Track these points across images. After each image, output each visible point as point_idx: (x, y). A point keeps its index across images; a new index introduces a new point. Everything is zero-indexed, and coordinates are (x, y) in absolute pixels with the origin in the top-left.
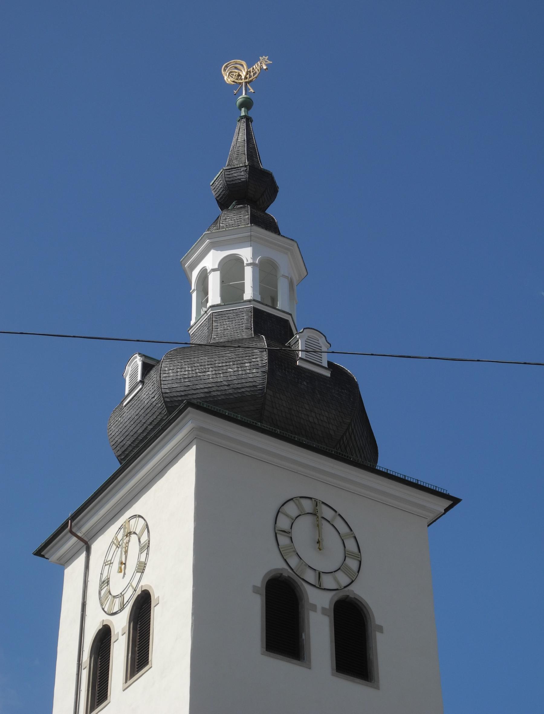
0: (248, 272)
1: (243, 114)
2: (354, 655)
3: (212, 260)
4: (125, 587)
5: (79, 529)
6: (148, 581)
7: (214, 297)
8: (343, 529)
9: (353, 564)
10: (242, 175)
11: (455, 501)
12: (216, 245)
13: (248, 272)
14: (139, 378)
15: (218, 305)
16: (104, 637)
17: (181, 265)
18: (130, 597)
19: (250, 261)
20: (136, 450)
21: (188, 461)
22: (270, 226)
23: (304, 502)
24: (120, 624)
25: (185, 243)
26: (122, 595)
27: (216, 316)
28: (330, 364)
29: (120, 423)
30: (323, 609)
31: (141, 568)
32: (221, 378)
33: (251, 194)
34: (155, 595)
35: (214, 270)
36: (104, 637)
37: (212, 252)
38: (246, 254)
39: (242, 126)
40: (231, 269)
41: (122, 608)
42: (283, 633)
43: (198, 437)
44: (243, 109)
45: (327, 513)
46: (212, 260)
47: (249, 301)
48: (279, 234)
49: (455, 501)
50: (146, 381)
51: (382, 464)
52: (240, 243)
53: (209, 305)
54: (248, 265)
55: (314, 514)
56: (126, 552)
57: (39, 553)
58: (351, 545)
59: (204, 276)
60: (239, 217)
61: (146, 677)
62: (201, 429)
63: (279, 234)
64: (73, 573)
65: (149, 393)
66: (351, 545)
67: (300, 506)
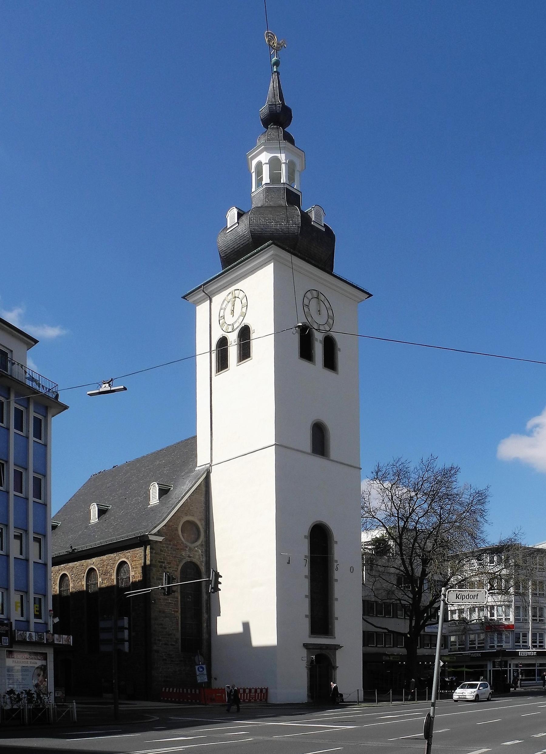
0: (283, 166)
1: (275, 70)
2: (330, 362)
3: (264, 157)
4: (235, 322)
5: (206, 290)
6: (246, 322)
7: (266, 179)
8: (328, 305)
9: (331, 321)
10: (279, 109)
11: (370, 295)
12: (267, 150)
13: (283, 166)
14: (236, 221)
15: (268, 184)
16: (223, 342)
17: (246, 157)
18: (238, 326)
19: (284, 161)
20: (236, 257)
21: (269, 269)
22: (288, 138)
23: (314, 292)
24: (233, 338)
25: (251, 145)
26: (233, 325)
27: (268, 190)
28: (325, 226)
29: (224, 240)
30: (317, 341)
31: (244, 315)
32: (278, 227)
33: (279, 118)
34: (252, 328)
35: (266, 163)
36: (223, 342)
37: (265, 153)
38: (282, 157)
39: (275, 76)
40: (274, 163)
41: (233, 330)
42: (306, 352)
43: (274, 259)
44: (275, 67)
45: (322, 298)
46: (264, 157)
47: (284, 183)
48: (294, 145)
49: (370, 295)
50: (240, 223)
51: (335, 271)
52: (280, 151)
53: (263, 183)
54: (284, 163)
55: (317, 298)
56: (234, 305)
57: (184, 298)
58: (330, 312)
59: (259, 165)
60: (274, 132)
61: (247, 364)
62: (276, 255)
63: (294, 145)
64: (202, 310)
65: (243, 228)
66: (330, 312)
67: (312, 294)
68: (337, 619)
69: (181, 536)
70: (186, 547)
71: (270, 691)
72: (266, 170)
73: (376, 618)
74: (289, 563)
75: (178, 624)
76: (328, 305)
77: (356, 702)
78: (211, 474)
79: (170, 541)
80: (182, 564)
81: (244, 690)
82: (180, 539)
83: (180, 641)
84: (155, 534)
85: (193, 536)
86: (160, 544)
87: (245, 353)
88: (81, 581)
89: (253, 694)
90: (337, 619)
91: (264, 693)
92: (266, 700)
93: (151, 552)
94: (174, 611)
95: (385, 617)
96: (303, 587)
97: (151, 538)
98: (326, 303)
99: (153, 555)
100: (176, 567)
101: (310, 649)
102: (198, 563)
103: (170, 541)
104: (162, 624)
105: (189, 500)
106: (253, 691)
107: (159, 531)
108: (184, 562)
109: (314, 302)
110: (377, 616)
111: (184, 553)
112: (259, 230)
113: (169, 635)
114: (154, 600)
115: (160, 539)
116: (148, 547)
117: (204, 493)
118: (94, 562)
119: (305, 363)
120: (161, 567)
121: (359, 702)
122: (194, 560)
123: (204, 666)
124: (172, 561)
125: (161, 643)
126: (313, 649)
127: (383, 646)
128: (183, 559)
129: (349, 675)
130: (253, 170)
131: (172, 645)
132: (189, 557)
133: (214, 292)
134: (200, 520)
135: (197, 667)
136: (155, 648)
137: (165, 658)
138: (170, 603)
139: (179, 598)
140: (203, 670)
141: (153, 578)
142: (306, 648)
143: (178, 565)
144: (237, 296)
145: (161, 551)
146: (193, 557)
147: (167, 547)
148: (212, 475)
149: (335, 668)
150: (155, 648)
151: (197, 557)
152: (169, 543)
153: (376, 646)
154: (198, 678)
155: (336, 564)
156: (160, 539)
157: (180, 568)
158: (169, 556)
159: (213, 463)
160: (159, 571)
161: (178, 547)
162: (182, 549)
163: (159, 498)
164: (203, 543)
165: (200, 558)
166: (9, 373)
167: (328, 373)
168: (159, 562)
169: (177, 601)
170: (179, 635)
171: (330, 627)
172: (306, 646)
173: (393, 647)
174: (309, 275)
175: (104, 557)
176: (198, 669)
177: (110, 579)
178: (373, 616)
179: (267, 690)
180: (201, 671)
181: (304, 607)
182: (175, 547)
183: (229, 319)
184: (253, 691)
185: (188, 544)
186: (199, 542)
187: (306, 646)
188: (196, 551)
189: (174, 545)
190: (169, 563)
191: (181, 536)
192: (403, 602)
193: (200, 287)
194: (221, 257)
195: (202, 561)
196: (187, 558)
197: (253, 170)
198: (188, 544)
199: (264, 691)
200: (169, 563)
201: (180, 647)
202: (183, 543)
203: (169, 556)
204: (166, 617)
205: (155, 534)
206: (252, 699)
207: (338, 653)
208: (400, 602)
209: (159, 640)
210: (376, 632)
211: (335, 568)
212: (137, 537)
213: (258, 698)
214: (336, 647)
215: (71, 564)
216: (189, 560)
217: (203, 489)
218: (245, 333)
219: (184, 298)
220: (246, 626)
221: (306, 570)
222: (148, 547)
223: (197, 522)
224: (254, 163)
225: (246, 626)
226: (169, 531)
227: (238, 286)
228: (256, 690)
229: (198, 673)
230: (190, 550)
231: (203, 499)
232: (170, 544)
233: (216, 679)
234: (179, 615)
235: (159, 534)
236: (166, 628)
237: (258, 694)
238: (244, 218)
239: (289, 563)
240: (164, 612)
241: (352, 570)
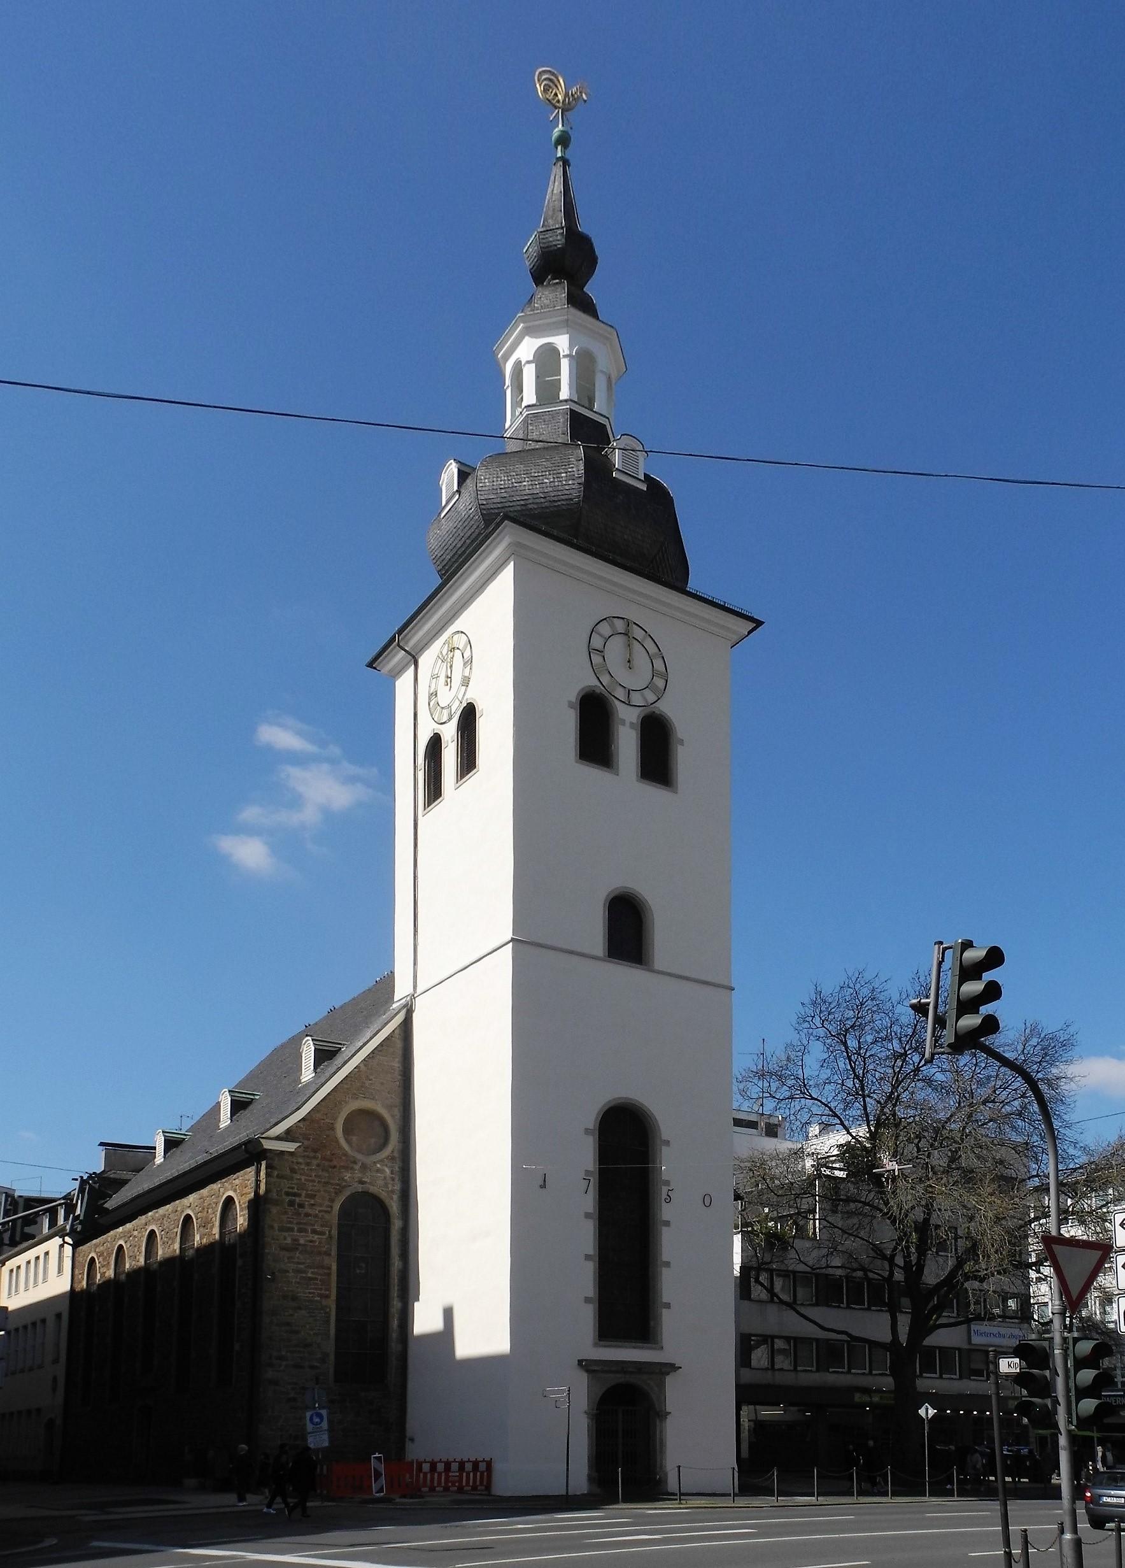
2: (657, 763)
5: (407, 643)
7: (530, 396)
8: (652, 649)
9: (660, 683)
16: (435, 743)
20: (455, 564)
26: (449, 707)
29: (439, 535)
30: (632, 723)
31: (466, 682)
35: (528, 362)
36: (435, 743)
42: (595, 745)
43: (516, 552)
45: (638, 633)
46: (527, 349)
50: (463, 491)
57: (370, 665)
61: (474, 779)
64: (403, 685)
65: (466, 504)
67: (612, 626)
68: (668, 1306)
69: (342, 1142)
70: (355, 1162)
71: (497, 1467)
72: (529, 375)
73: (848, 1311)
74: (543, 1186)
75: (328, 1322)
76: (652, 649)
77: (675, 1494)
78: (414, 1015)
79: (315, 1151)
80: (341, 1199)
81: (433, 1465)
82: (340, 1147)
83: (332, 1357)
84: (278, 1138)
85: (373, 1140)
86: (290, 1158)
87: (468, 762)
88: (173, 1243)
89: (455, 1474)
90: (668, 1306)
91: (483, 1470)
92: (488, 1487)
93: (267, 1175)
94: (321, 1296)
95: (869, 1309)
96: (582, 1236)
97: (267, 1145)
98: (649, 644)
99: (273, 1180)
100: (327, 1203)
101: (594, 1371)
102: (383, 1195)
103: (315, 1151)
104: (288, 1324)
105: (362, 1066)
106: (455, 1467)
107: (288, 1131)
108: (347, 1193)
109: (617, 643)
110: (848, 1307)
111: (347, 1176)
112: (498, 500)
114: (273, 1274)
115: (290, 1147)
116: (264, 1163)
117: (399, 1052)
118: (190, 1204)
119: (592, 773)
120: (291, 1203)
121: (681, 1494)
122: (373, 1189)
123: (324, 1412)
124: (319, 1191)
125: (284, 1363)
126: (604, 1372)
128: (345, 1187)
129: (701, 1426)
131: (312, 1367)
132: (361, 1182)
133: (422, 644)
134: (389, 1108)
135: (308, 1414)
136: (270, 1374)
137: (292, 1395)
138: (311, 1279)
139: (334, 1267)
140: (322, 1420)
141: (272, 1227)
142: (587, 1371)
143: (332, 1200)
144: (456, 646)
145: (293, 1171)
146: (370, 1183)
147: (308, 1164)
148: (416, 1017)
149: (663, 1415)
150: (270, 1374)
151: (381, 1182)
152: (312, 1154)
154: (310, 1440)
155: (664, 1189)
156: (290, 1147)
157: (337, 1207)
158: (313, 1181)
159: (419, 991)
160: (286, 1213)
161: (335, 1163)
162: (343, 1167)
163: (315, 1068)
164: (396, 1154)
165: (386, 1185)
166: (1084, 1159)
167: (653, 792)
168: (288, 1194)
169: (329, 1274)
170: (330, 1347)
171: (652, 1323)
172: (586, 1365)
173: (961, 1378)
174: (606, 589)
175: (204, 1192)
176: (311, 1419)
177: (210, 1234)
178: (839, 1307)
179: (489, 1464)
180: (317, 1424)
181: (582, 1279)
182: (327, 1163)
183: (445, 697)
184: (455, 1467)
185: (359, 1156)
186: (387, 1152)
187: (586, 1365)
188: (378, 1171)
189: (324, 1158)
190: (313, 1196)
191: (342, 1142)
192: (871, 1275)
193: (393, 639)
195: (393, 1192)
196: (356, 1185)
198: (359, 1156)
199: (482, 1467)
201: (332, 1370)
202: (345, 1154)
203: (313, 1181)
204: (300, 1308)
206: (453, 1485)
207: (669, 1380)
208: (866, 1275)
209: (280, 1358)
210: (817, 1340)
211: (664, 1196)
212: (239, 1146)
213: (481, 1484)
214: (672, 1368)
215: (162, 1211)
216: (360, 1188)
217: (399, 1044)
218: (468, 718)
219: (370, 665)
221: (588, 1202)
222: (264, 1163)
223: (382, 1114)
226: (312, 1132)
227: (458, 625)
228: (433, 1465)
229: (310, 1427)
230: (364, 1167)
231: (397, 1064)
232: (315, 1158)
233: (412, 1440)
234: (332, 1303)
235: (288, 1136)
236: (297, 1332)
237: (440, 1474)
238: (469, 482)
239: (543, 1186)
240: (294, 1298)
241: (707, 1201)
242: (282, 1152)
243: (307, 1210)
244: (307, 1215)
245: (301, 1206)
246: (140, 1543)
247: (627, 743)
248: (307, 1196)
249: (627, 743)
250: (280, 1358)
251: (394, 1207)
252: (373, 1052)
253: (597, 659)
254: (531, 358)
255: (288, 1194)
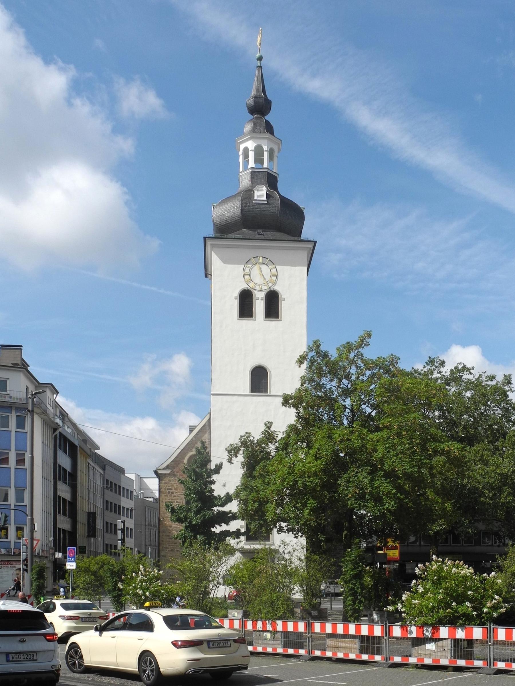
3: (251, 145)
7: (252, 164)
10: (262, 100)
35: (252, 150)
40: (259, 151)
46: (251, 145)
52: (266, 141)
59: (246, 151)
72: (252, 156)
84: (164, 469)
104: (169, 536)
113: (175, 543)
115: (168, 472)
119: (246, 323)
120: (169, 492)
127: (473, 544)
130: (241, 153)
141: (163, 502)
153: (450, 545)
160: (167, 496)
168: (168, 489)
173: (475, 545)
190: (176, 489)
194: (214, 223)
197: (241, 153)
200: (176, 489)
205: (164, 469)
209: (166, 548)
220: (233, 463)
224: (242, 147)
225: (233, 463)
242: (165, 474)
243: (175, 494)
244: (175, 496)
245: (172, 493)
246: (78, 603)
247: (259, 306)
248: (175, 489)
249: (259, 306)
250: (166, 548)
251: (28, 512)
252: (198, 432)
253: (247, 277)
254: (253, 149)
255: (168, 489)
